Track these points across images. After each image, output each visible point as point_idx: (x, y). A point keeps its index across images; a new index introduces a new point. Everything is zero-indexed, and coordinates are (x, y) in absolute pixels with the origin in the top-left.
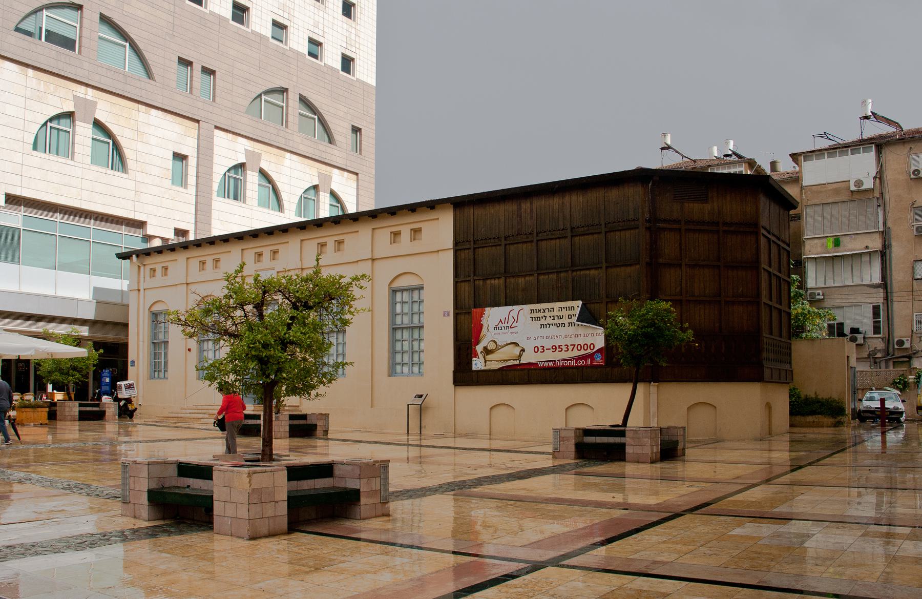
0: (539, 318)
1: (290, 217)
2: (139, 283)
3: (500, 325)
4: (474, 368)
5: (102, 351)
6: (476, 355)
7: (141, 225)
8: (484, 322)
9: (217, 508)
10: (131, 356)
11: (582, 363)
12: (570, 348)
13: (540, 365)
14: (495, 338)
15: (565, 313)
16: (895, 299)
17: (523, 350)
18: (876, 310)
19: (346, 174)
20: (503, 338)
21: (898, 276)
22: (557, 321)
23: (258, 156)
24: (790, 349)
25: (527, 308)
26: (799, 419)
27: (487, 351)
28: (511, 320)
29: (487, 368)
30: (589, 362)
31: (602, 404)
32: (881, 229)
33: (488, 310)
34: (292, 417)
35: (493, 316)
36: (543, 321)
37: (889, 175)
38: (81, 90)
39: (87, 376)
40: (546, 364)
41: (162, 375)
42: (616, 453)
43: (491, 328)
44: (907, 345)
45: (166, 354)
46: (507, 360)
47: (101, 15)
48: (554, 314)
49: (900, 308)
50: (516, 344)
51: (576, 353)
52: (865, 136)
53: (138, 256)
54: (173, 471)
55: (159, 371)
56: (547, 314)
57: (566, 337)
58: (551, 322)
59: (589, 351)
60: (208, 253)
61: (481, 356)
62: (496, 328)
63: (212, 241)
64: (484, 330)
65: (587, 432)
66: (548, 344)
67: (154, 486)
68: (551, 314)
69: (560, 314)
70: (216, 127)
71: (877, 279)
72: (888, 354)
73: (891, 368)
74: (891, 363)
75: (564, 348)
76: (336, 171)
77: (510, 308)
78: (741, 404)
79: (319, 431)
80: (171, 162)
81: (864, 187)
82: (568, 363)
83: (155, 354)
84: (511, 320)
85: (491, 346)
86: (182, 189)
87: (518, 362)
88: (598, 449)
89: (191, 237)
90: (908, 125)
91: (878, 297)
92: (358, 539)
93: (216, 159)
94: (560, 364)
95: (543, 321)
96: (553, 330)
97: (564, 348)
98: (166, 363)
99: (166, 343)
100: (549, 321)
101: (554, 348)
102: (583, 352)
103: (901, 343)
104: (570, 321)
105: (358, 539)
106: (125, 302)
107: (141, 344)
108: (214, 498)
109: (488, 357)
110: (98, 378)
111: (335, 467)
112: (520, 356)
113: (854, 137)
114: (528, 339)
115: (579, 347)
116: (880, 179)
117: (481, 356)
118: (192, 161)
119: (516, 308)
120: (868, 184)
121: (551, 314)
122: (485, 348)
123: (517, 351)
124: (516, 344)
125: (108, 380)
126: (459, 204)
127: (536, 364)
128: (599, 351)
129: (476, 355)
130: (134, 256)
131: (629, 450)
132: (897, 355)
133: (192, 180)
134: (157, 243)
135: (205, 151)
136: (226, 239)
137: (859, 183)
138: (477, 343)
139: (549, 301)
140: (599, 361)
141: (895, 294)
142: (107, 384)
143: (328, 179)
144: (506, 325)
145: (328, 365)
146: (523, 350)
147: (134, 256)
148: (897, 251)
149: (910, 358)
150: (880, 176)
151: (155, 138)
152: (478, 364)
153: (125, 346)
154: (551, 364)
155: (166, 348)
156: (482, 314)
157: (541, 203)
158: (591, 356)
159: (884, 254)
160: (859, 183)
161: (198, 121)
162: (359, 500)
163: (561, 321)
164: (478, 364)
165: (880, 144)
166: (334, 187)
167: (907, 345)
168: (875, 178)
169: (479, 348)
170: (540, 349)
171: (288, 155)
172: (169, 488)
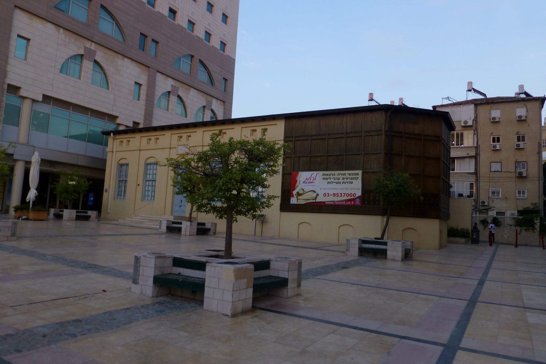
0: (327, 179)
1: (191, 119)
2: (113, 148)
3: (306, 181)
4: (291, 203)
5: (91, 183)
6: (293, 196)
7: (116, 117)
8: (298, 179)
9: (208, 292)
10: (106, 186)
11: (349, 203)
12: (343, 195)
13: (327, 203)
14: (303, 187)
15: (341, 177)
16: (481, 181)
17: (318, 195)
18: (471, 185)
19: (219, 102)
20: (307, 188)
21: (483, 170)
22: (336, 181)
23: (94, 52)
24: (449, 202)
25: (321, 173)
26: (452, 239)
27: (299, 194)
28: (312, 179)
29: (298, 203)
30: (353, 203)
31: (369, 226)
32: (476, 145)
33: (300, 172)
34: (199, 224)
35: (303, 176)
36: (329, 180)
37: (480, 119)
38: (88, 44)
39: (79, 194)
40: (330, 203)
41: (122, 197)
42: (381, 254)
43: (301, 183)
44: (486, 204)
45: (125, 187)
46: (308, 200)
47: (102, 5)
48: (336, 177)
49: (483, 185)
50: (314, 192)
51: (346, 198)
52: (469, 99)
53: (114, 134)
54: (170, 262)
55: (121, 195)
56: (331, 177)
57: (341, 189)
58: (333, 181)
59: (353, 197)
60: (153, 135)
61: (295, 196)
62: (304, 182)
63: (156, 129)
64: (298, 183)
65: (364, 242)
66: (331, 192)
67: (158, 273)
68: (334, 177)
69: (338, 177)
70: (158, 71)
71: (473, 171)
72: (477, 208)
73: (478, 215)
74: (478, 213)
75: (340, 195)
76: (214, 101)
77: (312, 172)
78: (429, 229)
79: (211, 232)
80: (134, 87)
81: (468, 124)
82: (341, 203)
83: (119, 186)
84: (312, 179)
85: (301, 192)
86: (138, 102)
87: (314, 201)
88: (373, 251)
89: (141, 126)
90: (490, 95)
91: (473, 179)
92: (300, 317)
93: (157, 88)
94: (337, 203)
95: (329, 180)
96: (334, 186)
97: (340, 195)
98: (125, 191)
99: (126, 181)
100: (332, 180)
101: (334, 195)
102: (349, 198)
103: (483, 202)
104: (343, 181)
105: (300, 317)
106: (104, 158)
107: (112, 181)
108: (206, 285)
109: (299, 197)
110: (86, 197)
111: (271, 263)
112: (316, 198)
113: (463, 99)
114: (321, 189)
115: (348, 195)
116: (476, 121)
117: (295, 196)
118: (144, 88)
119: (315, 173)
120: (470, 123)
121: (334, 177)
122: (298, 193)
123: (314, 195)
124: (314, 192)
125: (92, 199)
126: (288, 117)
127: (324, 202)
128: (359, 197)
129: (293, 196)
130: (112, 134)
131: (389, 253)
132: (481, 208)
133: (143, 96)
134: (122, 128)
135: (152, 84)
136: (163, 128)
137: (466, 122)
138: (294, 189)
139: (333, 170)
140: (358, 201)
141: (481, 178)
142: (91, 201)
143: (210, 103)
144: (309, 181)
145: (264, 197)
146: (318, 195)
147: (112, 134)
148: (483, 157)
149: (487, 210)
150: (476, 120)
151: (127, 73)
152: (293, 201)
153: (103, 181)
154: (333, 203)
155: (125, 183)
156: (297, 175)
157: (323, 121)
158: (354, 200)
159: (476, 157)
160: (466, 122)
161: (149, 67)
162: (287, 285)
163: (338, 181)
164: (293, 201)
165: (476, 103)
166: (213, 107)
167: (486, 204)
168: (473, 120)
169: (295, 192)
170: (327, 195)
171: (192, 90)
172: (167, 274)
